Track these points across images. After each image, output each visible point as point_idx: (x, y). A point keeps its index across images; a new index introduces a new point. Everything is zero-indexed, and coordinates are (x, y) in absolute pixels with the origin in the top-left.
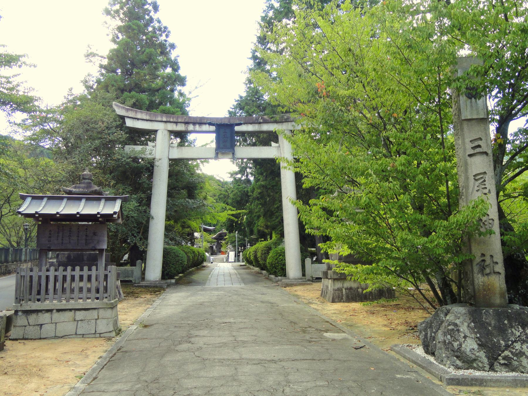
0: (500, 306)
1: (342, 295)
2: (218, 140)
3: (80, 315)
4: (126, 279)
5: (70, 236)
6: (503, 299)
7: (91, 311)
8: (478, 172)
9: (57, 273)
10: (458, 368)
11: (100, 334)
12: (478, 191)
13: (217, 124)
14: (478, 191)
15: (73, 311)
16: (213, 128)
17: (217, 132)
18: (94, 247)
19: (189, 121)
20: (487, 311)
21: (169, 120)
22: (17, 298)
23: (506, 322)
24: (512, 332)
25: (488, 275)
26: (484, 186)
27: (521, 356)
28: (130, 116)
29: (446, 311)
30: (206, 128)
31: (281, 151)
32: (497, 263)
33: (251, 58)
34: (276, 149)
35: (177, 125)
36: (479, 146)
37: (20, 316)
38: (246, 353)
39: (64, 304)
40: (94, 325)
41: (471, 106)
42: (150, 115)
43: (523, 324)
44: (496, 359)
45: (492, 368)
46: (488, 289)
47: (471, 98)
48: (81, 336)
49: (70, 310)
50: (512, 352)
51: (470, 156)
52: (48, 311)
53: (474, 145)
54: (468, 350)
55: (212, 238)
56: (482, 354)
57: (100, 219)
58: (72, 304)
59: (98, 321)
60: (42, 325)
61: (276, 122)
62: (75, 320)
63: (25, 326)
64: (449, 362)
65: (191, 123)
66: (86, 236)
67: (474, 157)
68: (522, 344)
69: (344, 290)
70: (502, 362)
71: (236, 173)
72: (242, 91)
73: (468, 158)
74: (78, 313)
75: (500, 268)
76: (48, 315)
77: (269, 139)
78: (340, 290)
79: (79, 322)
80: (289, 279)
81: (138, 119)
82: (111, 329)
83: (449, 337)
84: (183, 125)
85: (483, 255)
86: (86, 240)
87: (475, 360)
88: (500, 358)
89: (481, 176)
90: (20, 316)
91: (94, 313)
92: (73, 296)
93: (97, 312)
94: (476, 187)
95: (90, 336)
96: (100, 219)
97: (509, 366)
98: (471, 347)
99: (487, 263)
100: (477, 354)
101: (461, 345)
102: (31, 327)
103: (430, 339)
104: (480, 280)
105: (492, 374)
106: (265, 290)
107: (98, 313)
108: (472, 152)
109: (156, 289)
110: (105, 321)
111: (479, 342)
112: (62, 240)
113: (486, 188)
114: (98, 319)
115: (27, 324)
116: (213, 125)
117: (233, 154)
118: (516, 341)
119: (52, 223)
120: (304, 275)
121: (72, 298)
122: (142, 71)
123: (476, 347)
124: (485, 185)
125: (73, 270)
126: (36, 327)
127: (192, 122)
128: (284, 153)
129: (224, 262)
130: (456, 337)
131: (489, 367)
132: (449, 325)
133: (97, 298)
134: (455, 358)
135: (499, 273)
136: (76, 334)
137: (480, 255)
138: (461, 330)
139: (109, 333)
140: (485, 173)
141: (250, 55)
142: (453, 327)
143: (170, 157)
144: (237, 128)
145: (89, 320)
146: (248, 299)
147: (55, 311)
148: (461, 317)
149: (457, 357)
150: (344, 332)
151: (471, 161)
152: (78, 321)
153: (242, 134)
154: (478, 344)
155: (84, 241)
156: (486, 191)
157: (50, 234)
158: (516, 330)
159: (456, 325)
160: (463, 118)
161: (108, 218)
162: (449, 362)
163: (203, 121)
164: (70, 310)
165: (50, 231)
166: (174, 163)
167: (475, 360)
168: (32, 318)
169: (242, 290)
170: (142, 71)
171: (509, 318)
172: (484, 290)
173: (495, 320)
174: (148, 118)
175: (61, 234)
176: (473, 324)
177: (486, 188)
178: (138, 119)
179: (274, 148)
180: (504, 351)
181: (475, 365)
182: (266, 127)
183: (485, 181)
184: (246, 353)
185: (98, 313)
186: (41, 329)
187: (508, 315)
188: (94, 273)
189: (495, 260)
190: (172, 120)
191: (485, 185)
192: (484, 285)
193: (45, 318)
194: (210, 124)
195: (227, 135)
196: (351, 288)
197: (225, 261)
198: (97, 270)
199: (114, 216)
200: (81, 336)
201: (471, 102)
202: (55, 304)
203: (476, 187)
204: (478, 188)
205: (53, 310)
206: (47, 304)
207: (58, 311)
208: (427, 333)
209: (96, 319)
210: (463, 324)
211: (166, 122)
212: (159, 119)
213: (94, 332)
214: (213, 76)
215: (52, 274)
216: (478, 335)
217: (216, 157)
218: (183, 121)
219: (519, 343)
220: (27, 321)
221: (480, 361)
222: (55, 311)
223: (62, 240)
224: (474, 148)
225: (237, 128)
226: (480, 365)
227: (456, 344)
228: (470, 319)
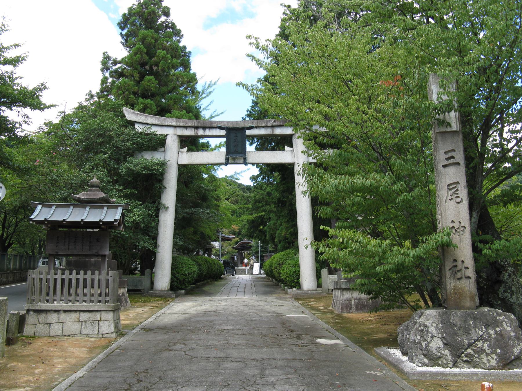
0: (469, 308)
1: (351, 305)
3: (84, 316)
4: (135, 288)
6: (472, 302)
8: (452, 182)
9: (64, 277)
10: (424, 365)
12: (450, 200)
13: (227, 128)
14: (450, 200)
15: (78, 312)
16: (223, 132)
19: (200, 125)
20: (455, 313)
23: (471, 323)
24: (476, 331)
25: (459, 279)
26: (456, 196)
27: (482, 354)
29: (420, 314)
31: (296, 156)
34: (290, 153)
36: (453, 157)
38: (234, 353)
39: (69, 306)
40: (96, 326)
43: (486, 325)
44: (460, 357)
45: (455, 365)
46: (458, 292)
48: (85, 336)
49: (76, 311)
50: (473, 350)
51: (444, 166)
53: (447, 156)
54: (434, 349)
55: (233, 248)
56: (447, 352)
57: (103, 227)
58: (77, 306)
59: (101, 323)
60: (50, 324)
63: (36, 324)
64: (417, 360)
65: (201, 127)
67: (448, 168)
68: (484, 343)
69: (353, 301)
70: (465, 359)
71: (258, 176)
75: (471, 272)
76: (55, 315)
77: (284, 142)
78: (349, 300)
79: (84, 323)
80: (303, 290)
82: (113, 330)
83: (419, 337)
87: (440, 358)
88: (463, 355)
89: (455, 186)
92: (78, 298)
93: (99, 314)
94: (449, 196)
95: (93, 336)
96: (103, 227)
97: (470, 362)
99: (459, 268)
100: (443, 352)
101: (429, 343)
102: (41, 326)
104: (451, 283)
105: (456, 370)
106: (276, 302)
108: (446, 163)
109: (164, 297)
110: (106, 323)
111: (444, 341)
113: (459, 197)
114: (101, 320)
115: (38, 322)
117: (245, 159)
118: (478, 340)
119: (60, 230)
120: (319, 285)
121: (78, 301)
122: (153, 66)
123: (441, 345)
124: (458, 194)
125: (78, 274)
126: (46, 325)
127: (202, 126)
128: (298, 157)
129: (245, 274)
130: (425, 337)
131: (452, 364)
132: (420, 326)
134: (423, 356)
136: (81, 333)
137: (452, 261)
139: (110, 334)
140: (458, 183)
142: (423, 328)
143: (179, 163)
144: (248, 132)
146: (255, 309)
148: (431, 319)
149: (425, 355)
150: (338, 338)
151: (445, 172)
152: (82, 321)
153: (252, 137)
154: (444, 343)
158: (479, 330)
159: (425, 326)
161: (110, 225)
162: (417, 360)
164: (76, 311)
165: (58, 237)
166: (183, 169)
167: (440, 358)
168: (42, 317)
169: (252, 301)
170: (153, 66)
171: (475, 319)
173: (462, 321)
176: (441, 325)
177: (459, 197)
179: (288, 153)
180: (466, 349)
181: (440, 362)
182: (278, 131)
184: (234, 353)
185: (101, 315)
186: (50, 327)
187: (474, 317)
188: (96, 277)
191: (458, 194)
192: (455, 289)
193: (53, 318)
194: (221, 128)
195: (236, 140)
197: (247, 273)
198: (99, 274)
199: (115, 224)
200: (85, 336)
203: (449, 196)
204: (451, 197)
206: (55, 305)
207: (65, 311)
210: (432, 325)
214: (226, 74)
215: (59, 276)
217: (226, 163)
218: (193, 125)
219: (481, 342)
221: (445, 359)
224: (447, 159)
225: (248, 132)
226: (445, 362)
228: (438, 321)
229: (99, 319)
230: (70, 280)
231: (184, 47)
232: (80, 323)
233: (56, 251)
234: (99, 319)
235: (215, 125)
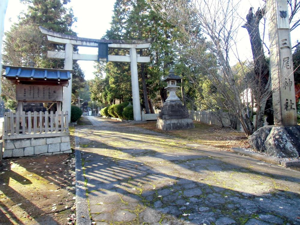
2: (99, 52)
3: (49, 141)
5: (38, 93)
7: (56, 138)
11: (63, 151)
15: (45, 139)
16: (97, 45)
17: (99, 46)
18: (55, 100)
21: (72, 38)
22: (6, 132)
28: (50, 34)
30: (92, 44)
32: (293, 104)
33: (113, 11)
35: (77, 42)
37: (9, 143)
39: (38, 134)
41: (283, 22)
42: (62, 35)
47: (282, 18)
49: (43, 138)
52: (28, 139)
59: (62, 144)
60: (24, 148)
61: (129, 44)
62: (46, 144)
63: (13, 149)
66: (49, 93)
72: (109, 27)
73: (281, 49)
74: (48, 140)
76: (28, 142)
78: (169, 124)
79: (49, 145)
80: (135, 121)
81: (55, 37)
84: (80, 42)
85: (287, 100)
86: (49, 95)
90: (9, 143)
91: (58, 140)
93: (60, 139)
98: (290, 146)
101: (285, 145)
102: (17, 150)
103: (261, 144)
107: (61, 139)
112: (34, 95)
113: (288, 65)
115: (14, 148)
116: (97, 43)
123: (292, 146)
126: (21, 149)
133: (60, 131)
135: (294, 109)
136: (48, 152)
138: (284, 138)
141: (113, 9)
143: (74, 59)
145: (55, 144)
147: (33, 139)
152: (48, 144)
155: (48, 96)
156: (288, 67)
157: (25, 91)
160: (278, 28)
163: (91, 41)
164: (43, 138)
165: (25, 89)
168: (18, 144)
172: (288, 118)
174: (60, 36)
175: (32, 91)
176: (288, 135)
178: (55, 37)
181: (292, 155)
183: (288, 62)
185: (61, 139)
189: (292, 102)
190: (74, 39)
194: (95, 42)
196: (174, 124)
201: (283, 19)
202: (32, 134)
205: (31, 138)
207: (35, 139)
208: (258, 141)
209: (60, 143)
211: (71, 39)
212: (67, 37)
213: (59, 150)
216: (292, 140)
220: (14, 146)
222: (33, 139)
223: (34, 95)
227: (281, 145)
229: (60, 142)
230: (38, 118)
231: (6, 50)
232: (47, 145)
233: (24, 99)
234: (60, 142)
235: (92, 41)
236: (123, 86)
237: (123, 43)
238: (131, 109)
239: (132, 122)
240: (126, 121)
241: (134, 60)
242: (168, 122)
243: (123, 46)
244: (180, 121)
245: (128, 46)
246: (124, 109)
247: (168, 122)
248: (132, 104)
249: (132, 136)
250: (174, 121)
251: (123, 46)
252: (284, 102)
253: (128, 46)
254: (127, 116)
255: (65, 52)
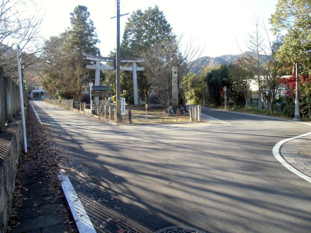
78: (150, 107)
80: (135, 105)
81: (90, 57)
174: (93, 57)
236: (128, 83)
237: (128, 60)
238: (133, 98)
239: (133, 106)
240: (130, 105)
241: (135, 69)
242: (150, 105)
243: (129, 61)
244: (156, 105)
245: (131, 61)
246: (129, 98)
247: (150, 105)
248: (133, 95)
249: (220, 202)
250: (153, 105)
251: (129, 61)
252: (174, 99)
253: (131, 61)
254: (130, 102)
255: (96, 66)
